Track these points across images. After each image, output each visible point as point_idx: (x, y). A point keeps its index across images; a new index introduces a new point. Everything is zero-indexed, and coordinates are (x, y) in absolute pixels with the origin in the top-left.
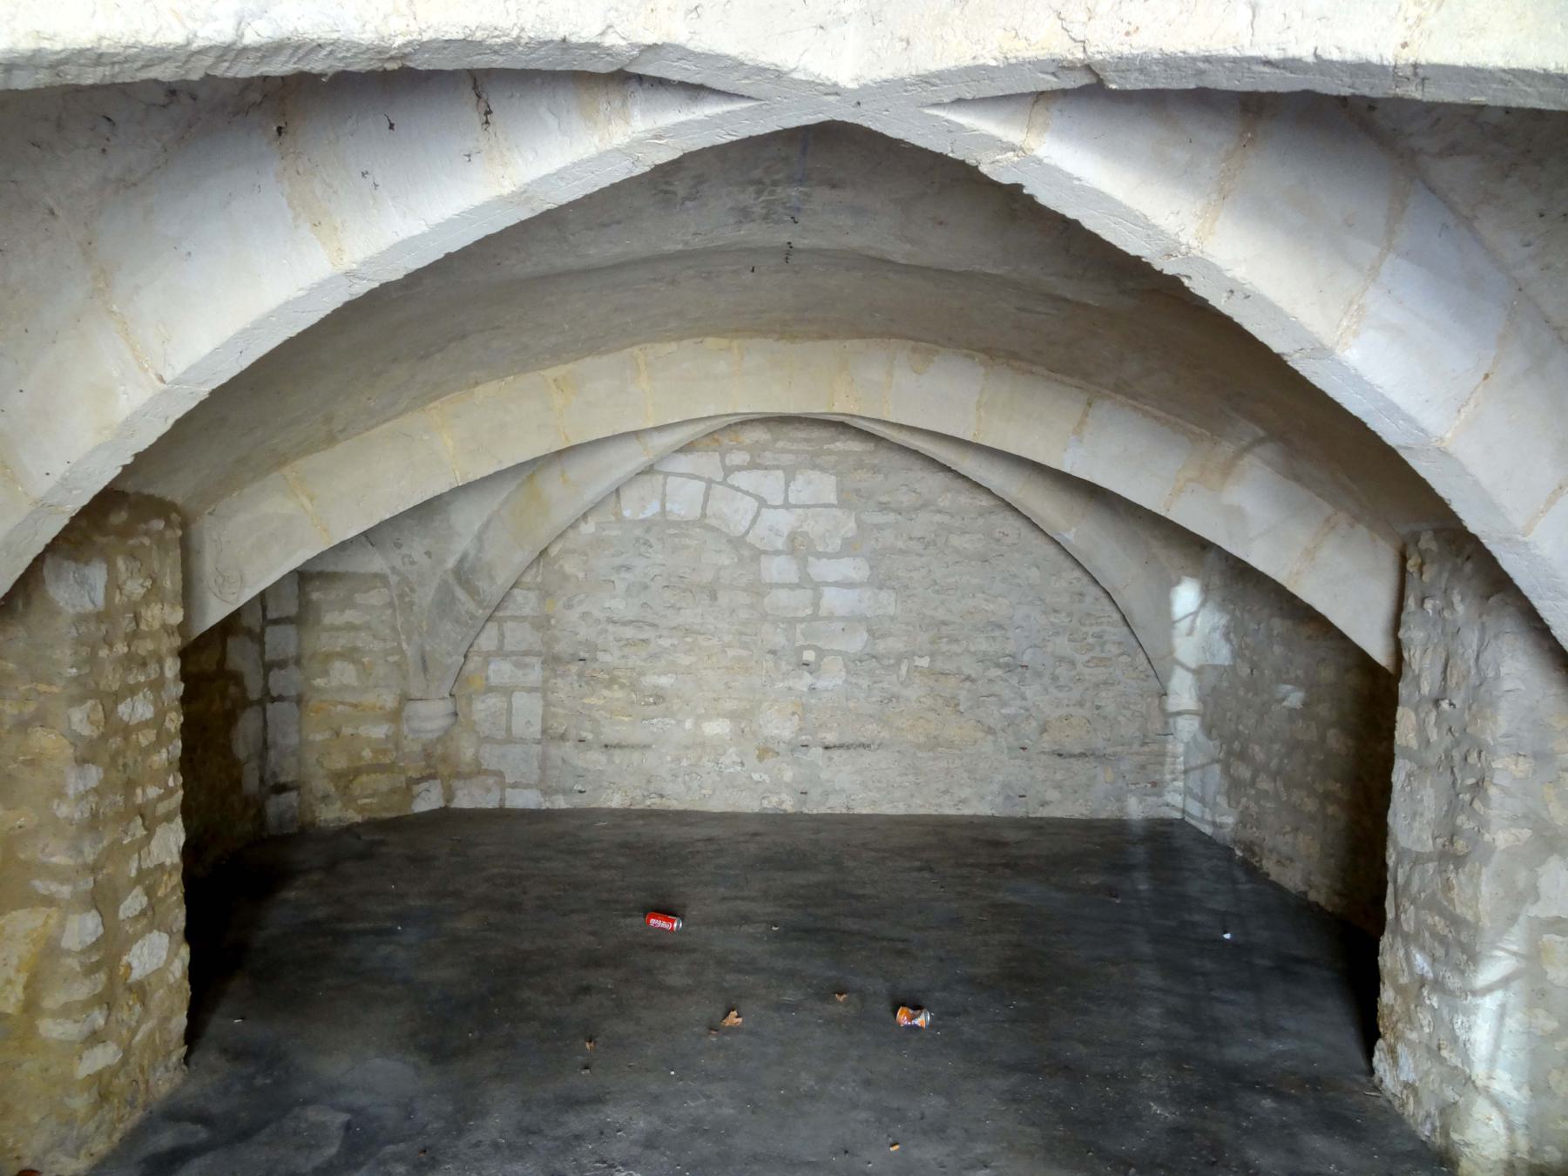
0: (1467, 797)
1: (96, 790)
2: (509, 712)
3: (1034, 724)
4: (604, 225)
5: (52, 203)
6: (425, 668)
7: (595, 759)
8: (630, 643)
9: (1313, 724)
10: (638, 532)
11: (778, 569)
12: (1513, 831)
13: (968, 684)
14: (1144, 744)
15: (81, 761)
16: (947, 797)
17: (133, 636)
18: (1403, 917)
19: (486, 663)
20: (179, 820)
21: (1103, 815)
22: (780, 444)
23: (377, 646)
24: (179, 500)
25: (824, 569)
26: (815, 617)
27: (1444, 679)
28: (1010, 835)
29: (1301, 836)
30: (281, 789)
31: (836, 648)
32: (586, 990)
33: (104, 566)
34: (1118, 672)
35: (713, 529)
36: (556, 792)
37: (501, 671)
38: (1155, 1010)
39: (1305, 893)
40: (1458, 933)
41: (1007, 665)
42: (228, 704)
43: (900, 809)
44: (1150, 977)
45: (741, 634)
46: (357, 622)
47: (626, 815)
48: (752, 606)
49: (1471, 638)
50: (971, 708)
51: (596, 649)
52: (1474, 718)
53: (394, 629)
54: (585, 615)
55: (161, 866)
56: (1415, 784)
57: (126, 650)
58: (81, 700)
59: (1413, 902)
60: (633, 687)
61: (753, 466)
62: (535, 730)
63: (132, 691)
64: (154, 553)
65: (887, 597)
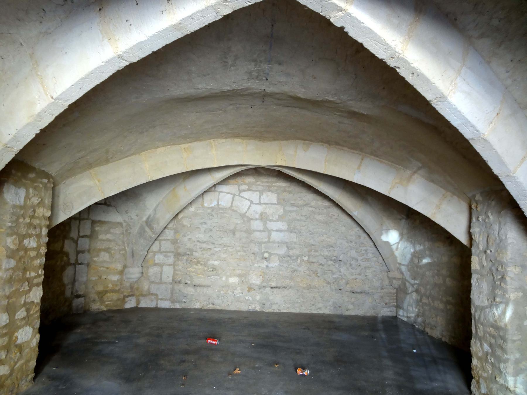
0: (498, 283)
1: (13, 268)
2: (161, 273)
3: (344, 281)
4: (204, 76)
5: (22, 41)
6: (133, 256)
7: (191, 290)
8: (205, 249)
9: (441, 277)
10: (209, 211)
11: (257, 225)
12: (516, 293)
13: (321, 266)
14: (382, 289)
15: (8, 257)
16: (314, 307)
17: (32, 217)
18: (478, 330)
19: (154, 255)
20: (41, 287)
21: (369, 315)
22: (258, 183)
23: (117, 248)
24: (53, 175)
25: (272, 225)
26: (269, 242)
27: (488, 243)
28: (336, 320)
29: (438, 318)
30: (78, 296)
31: (275, 252)
32: (184, 361)
33: (25, 190)
34: (373, 263)
35: (234, 211)
36: (176, 302)
37: (159, 258)
38: (391, 372)
39: (441, 339)
40: (499, 332)
41: (334, 260)
42: (63, 263)
43: (297, 311)
44: (387, 362)
45: (243, 247)
46: (111, 238)
47: (201, 310)
48: (247, 238)
49: (496, 227)
50: (322, 275)
51: (193, 251)
52: (499, 254)
53: (123, 242)
54: (189, 240)
55: (33, 302)
56: (480, 282)
57: (29, 221)
58: (11, 235)
59: (482, 324)
60: (205, 265)
61: (249, 190)
62: (170, 279)
63: (30, 236)
64: (43, 190)
65: (293, 235)
